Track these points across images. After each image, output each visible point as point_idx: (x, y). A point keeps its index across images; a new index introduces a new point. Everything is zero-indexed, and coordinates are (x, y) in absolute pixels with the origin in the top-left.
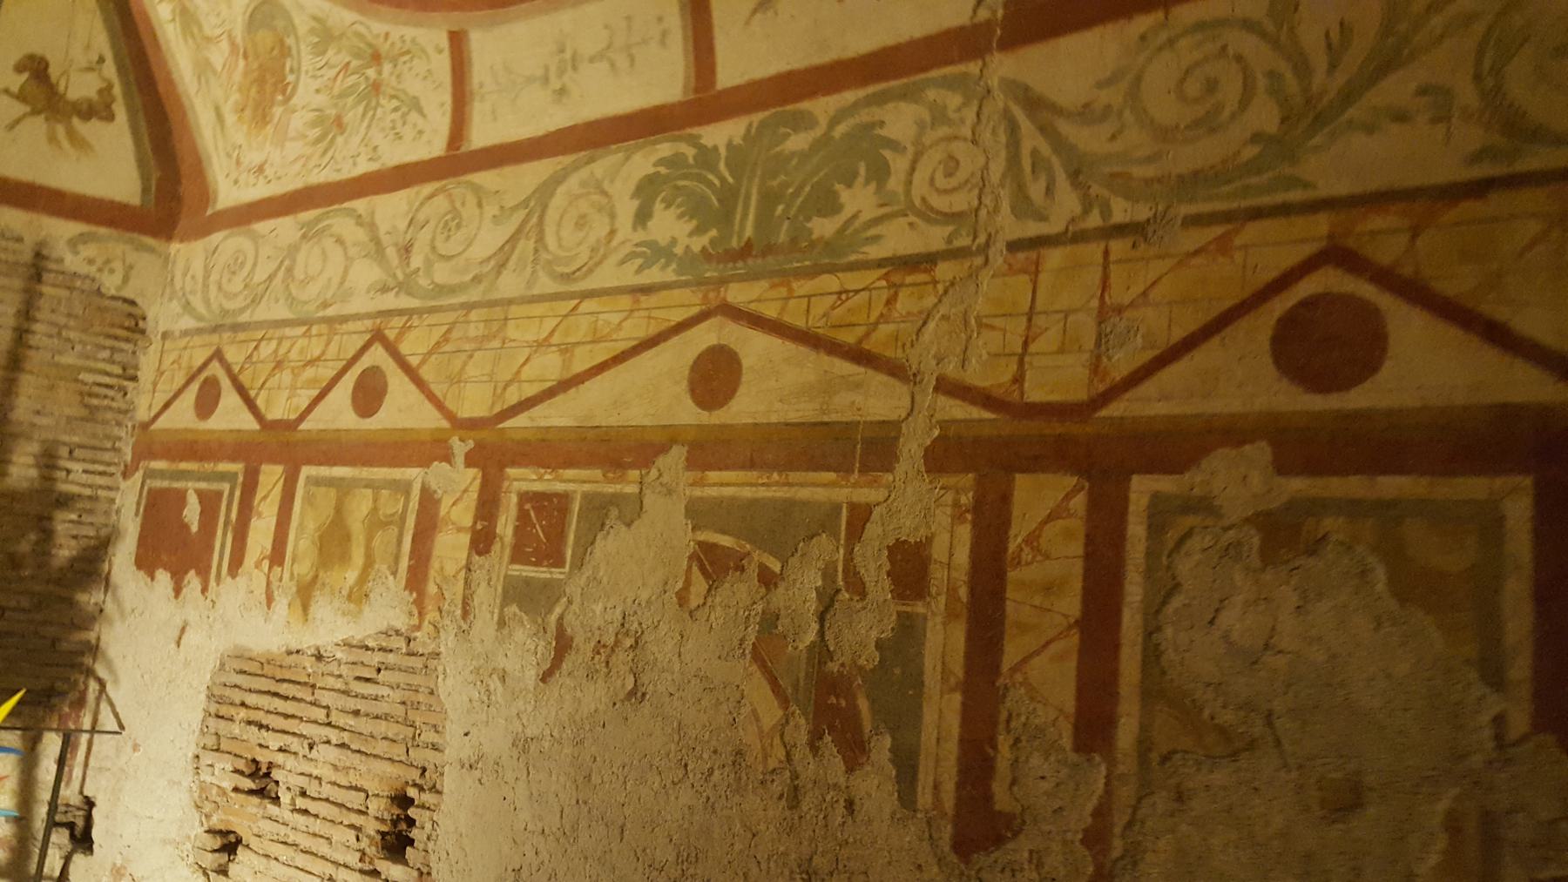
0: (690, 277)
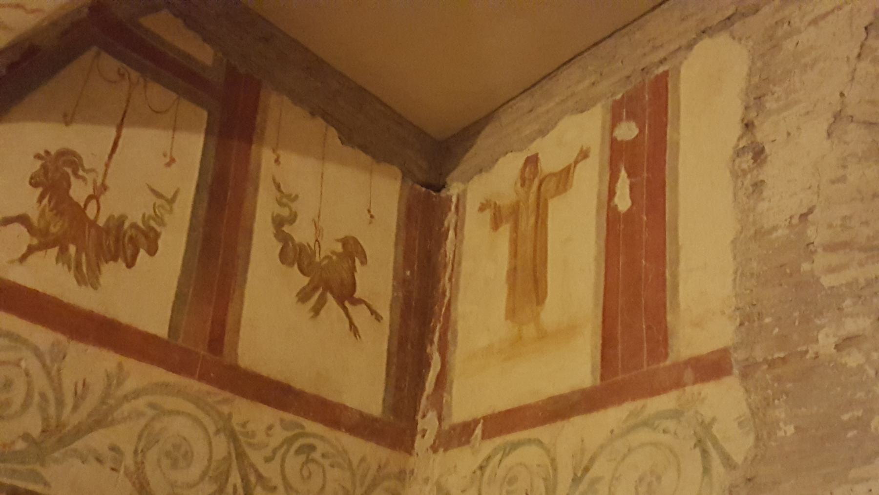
0: (624, 110)
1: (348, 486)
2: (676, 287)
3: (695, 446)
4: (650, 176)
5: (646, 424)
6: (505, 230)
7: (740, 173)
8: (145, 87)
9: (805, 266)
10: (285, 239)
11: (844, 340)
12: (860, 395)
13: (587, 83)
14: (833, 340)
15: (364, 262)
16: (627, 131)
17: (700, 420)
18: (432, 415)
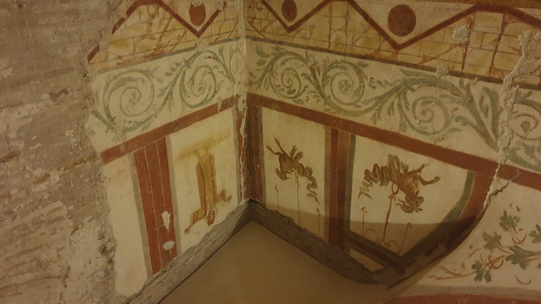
0: (171, 254)
1: (272, 78)
2: (135, 185)
3: (114, 118)
4: (154, 230)
5: (140, 124)
6: (219, 190)
7: (112, 240)
8: (378, 240)
9: (71, 208)
10: (311, 178)
11: (46, 179)
12: (32, 157)
13: (190, 260)
14: (52, 178)
15: (277, 170)
16: (168, 245)
17: (113, 130)
18: (241, 109)
